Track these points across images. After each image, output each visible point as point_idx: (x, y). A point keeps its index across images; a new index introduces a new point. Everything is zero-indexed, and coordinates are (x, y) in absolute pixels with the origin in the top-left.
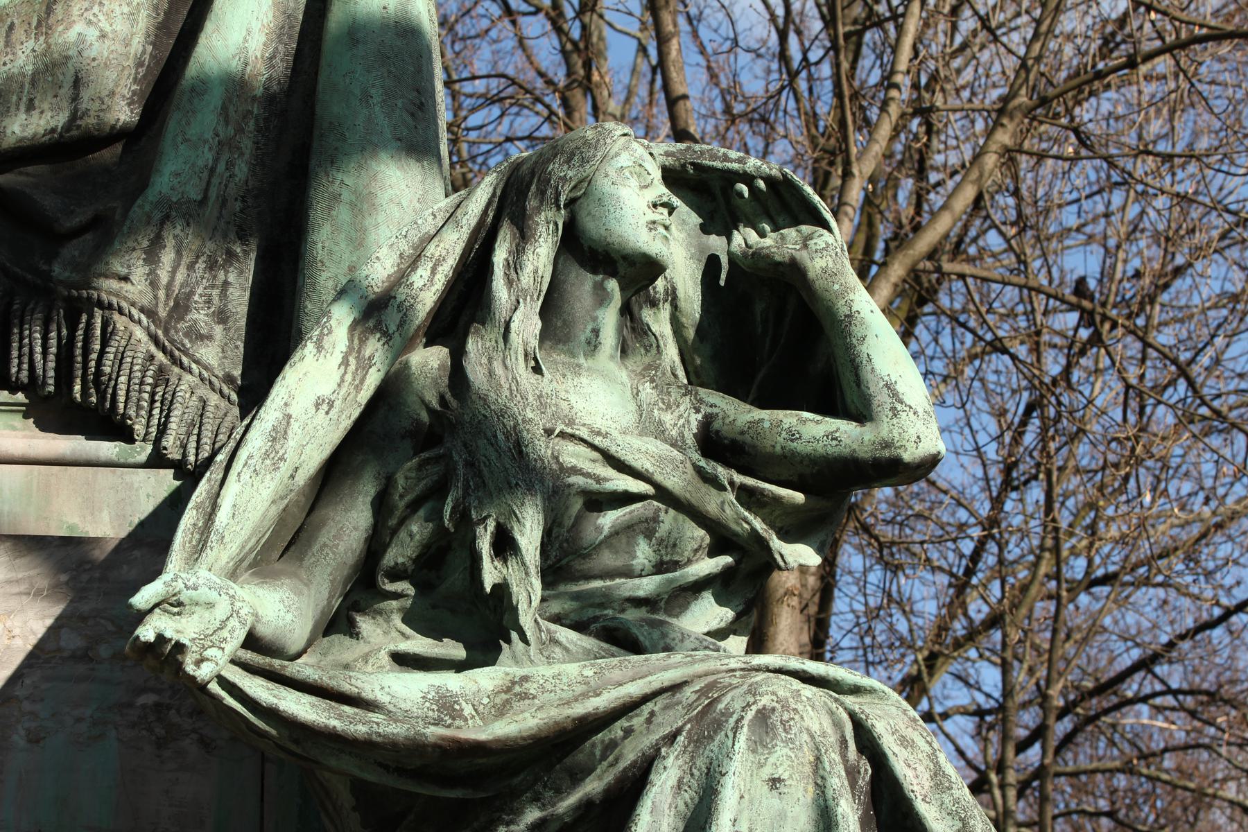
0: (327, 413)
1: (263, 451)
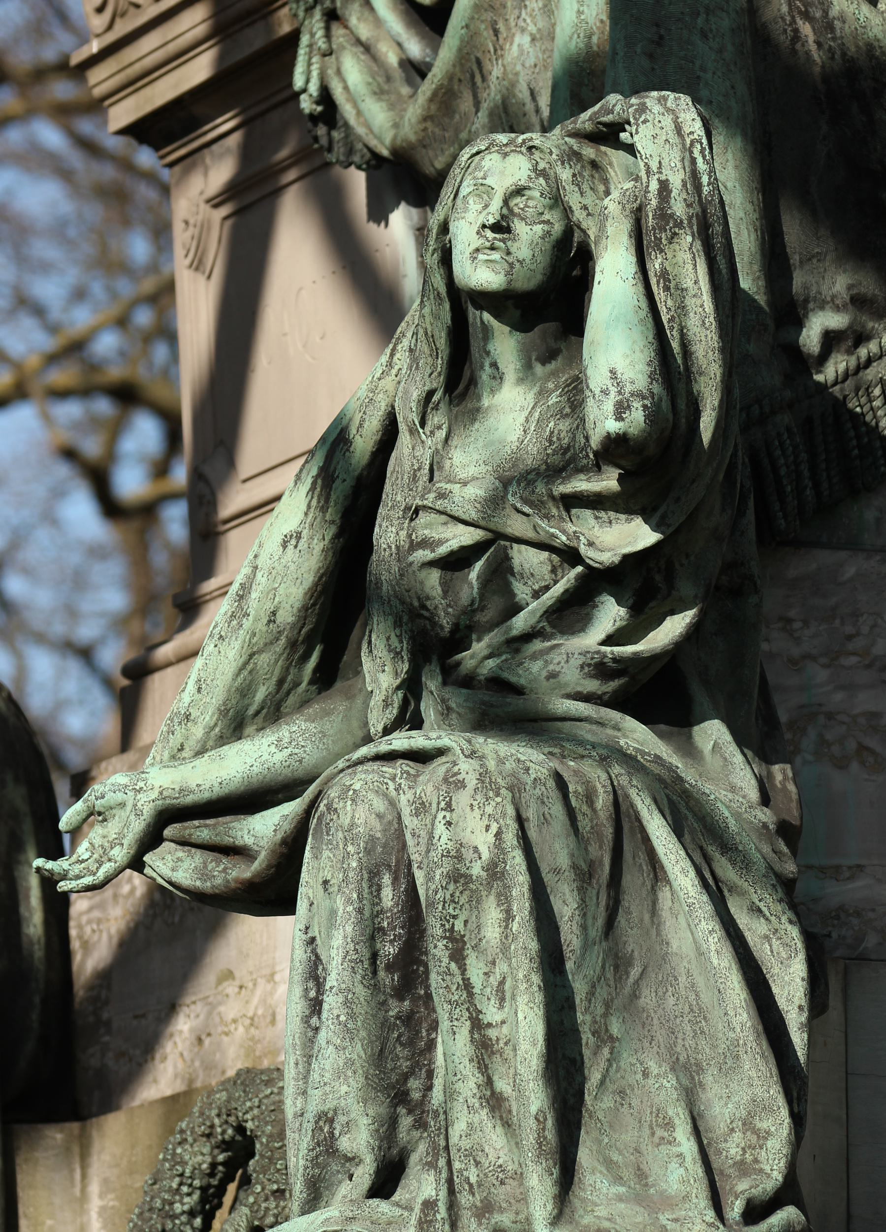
0: (296, 547)
1: (230, 613)
